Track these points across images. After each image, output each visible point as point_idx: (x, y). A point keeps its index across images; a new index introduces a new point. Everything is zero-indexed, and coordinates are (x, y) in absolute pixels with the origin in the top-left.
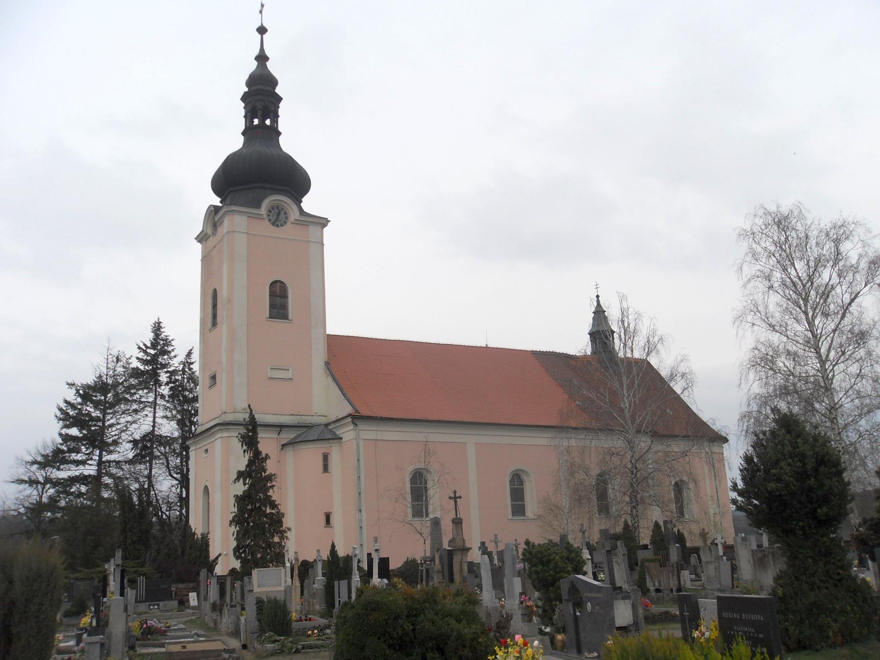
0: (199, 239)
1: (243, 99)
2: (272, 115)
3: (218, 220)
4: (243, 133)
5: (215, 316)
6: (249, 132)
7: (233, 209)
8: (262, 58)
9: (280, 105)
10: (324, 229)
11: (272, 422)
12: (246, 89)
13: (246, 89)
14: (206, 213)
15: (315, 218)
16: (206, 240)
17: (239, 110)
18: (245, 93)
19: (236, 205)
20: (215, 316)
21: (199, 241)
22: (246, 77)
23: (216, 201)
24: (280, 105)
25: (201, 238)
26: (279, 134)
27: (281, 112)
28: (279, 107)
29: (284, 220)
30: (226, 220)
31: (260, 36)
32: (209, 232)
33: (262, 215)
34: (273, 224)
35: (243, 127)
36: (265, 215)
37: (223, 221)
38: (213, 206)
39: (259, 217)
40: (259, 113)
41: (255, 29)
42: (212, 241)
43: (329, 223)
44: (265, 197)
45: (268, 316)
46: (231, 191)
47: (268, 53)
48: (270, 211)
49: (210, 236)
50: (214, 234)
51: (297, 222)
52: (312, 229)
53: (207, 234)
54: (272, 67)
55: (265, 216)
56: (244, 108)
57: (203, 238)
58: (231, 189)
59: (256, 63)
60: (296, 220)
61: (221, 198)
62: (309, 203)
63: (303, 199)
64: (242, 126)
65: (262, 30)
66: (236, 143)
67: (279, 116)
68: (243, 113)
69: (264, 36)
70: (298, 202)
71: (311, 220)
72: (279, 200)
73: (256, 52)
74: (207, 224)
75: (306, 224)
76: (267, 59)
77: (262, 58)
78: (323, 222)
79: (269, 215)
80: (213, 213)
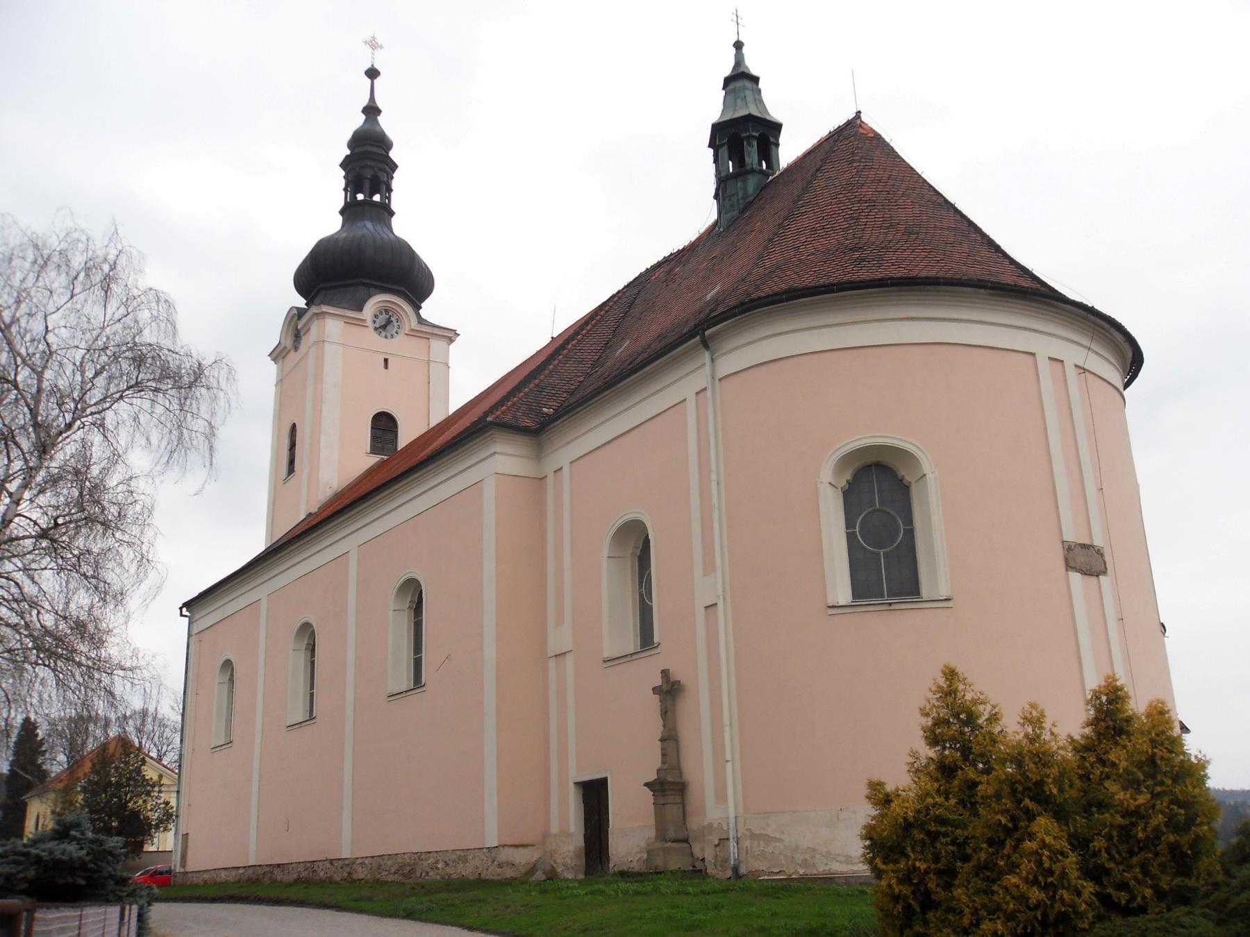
0: (274, 355)
1: (344, 165)
2: (384, 188)
3: (302, 328)
4: (342, 212)
5: (292, 462)
6: (350, 211)
7: (324, 310)
8: (371, 111)
9: (395, 175)
10: (451, 346)
11: (351, 480)
12: (348, 152)
13: (348, 152)
14: (286, 319)
15: (435, 329)
16: (283, 358)
17: (337, 180)
18: (347, 156)
19: (329, 304)
20: (292, 462)
21: (275, 360)
22: (349, 136)
23: (301, 302)
24: (394, 175)
25: (278, 355)
26: (392, 214)
27: (395, 184)
28: (392, 178)
29: (380, 317)
30: (314, 327)
31: (369, 81)
32: (289, 343)
33: (365, 320)
34: (814, 850)
35: (341, 204)
36: (368, 321)
37: (309, 329)
38: (297, 308)
39: (361, 323)
40: (367, 185)
41: (364, 72)
42: (293, 357)
43: (458, 338)
44: (370, 297)
45: (369, 450)
46: (321, 289)
47: (380, 103)
48: (376, 316)
49: (290, 351)
50: (296, 348)
51: (414, 334)
52: (437, 345)
53: (285, 348)
54: (386, 123)
55: (369, 323)
56: (344, 177)
57: (279, 354)
58: (321, 285)
59: (363, 117)
60: (412, 330)
61: (305, 299)
62: (429, 309)
63: (423, 305)
64: (339, 200)
65: (372, 73)
66: (330, 224)
67: (392, 190)
68: (342, 183)
69: (375, 81)
70: (417, 308)
71: (436, 331)
72: (394, 303)
73: (365, 101)
74: (287, 330)
75: (427, 337)
76: (378, 111)
77: (371, 111)
78: (450, 336)
79: (375, 322)
80: (296, 318)
